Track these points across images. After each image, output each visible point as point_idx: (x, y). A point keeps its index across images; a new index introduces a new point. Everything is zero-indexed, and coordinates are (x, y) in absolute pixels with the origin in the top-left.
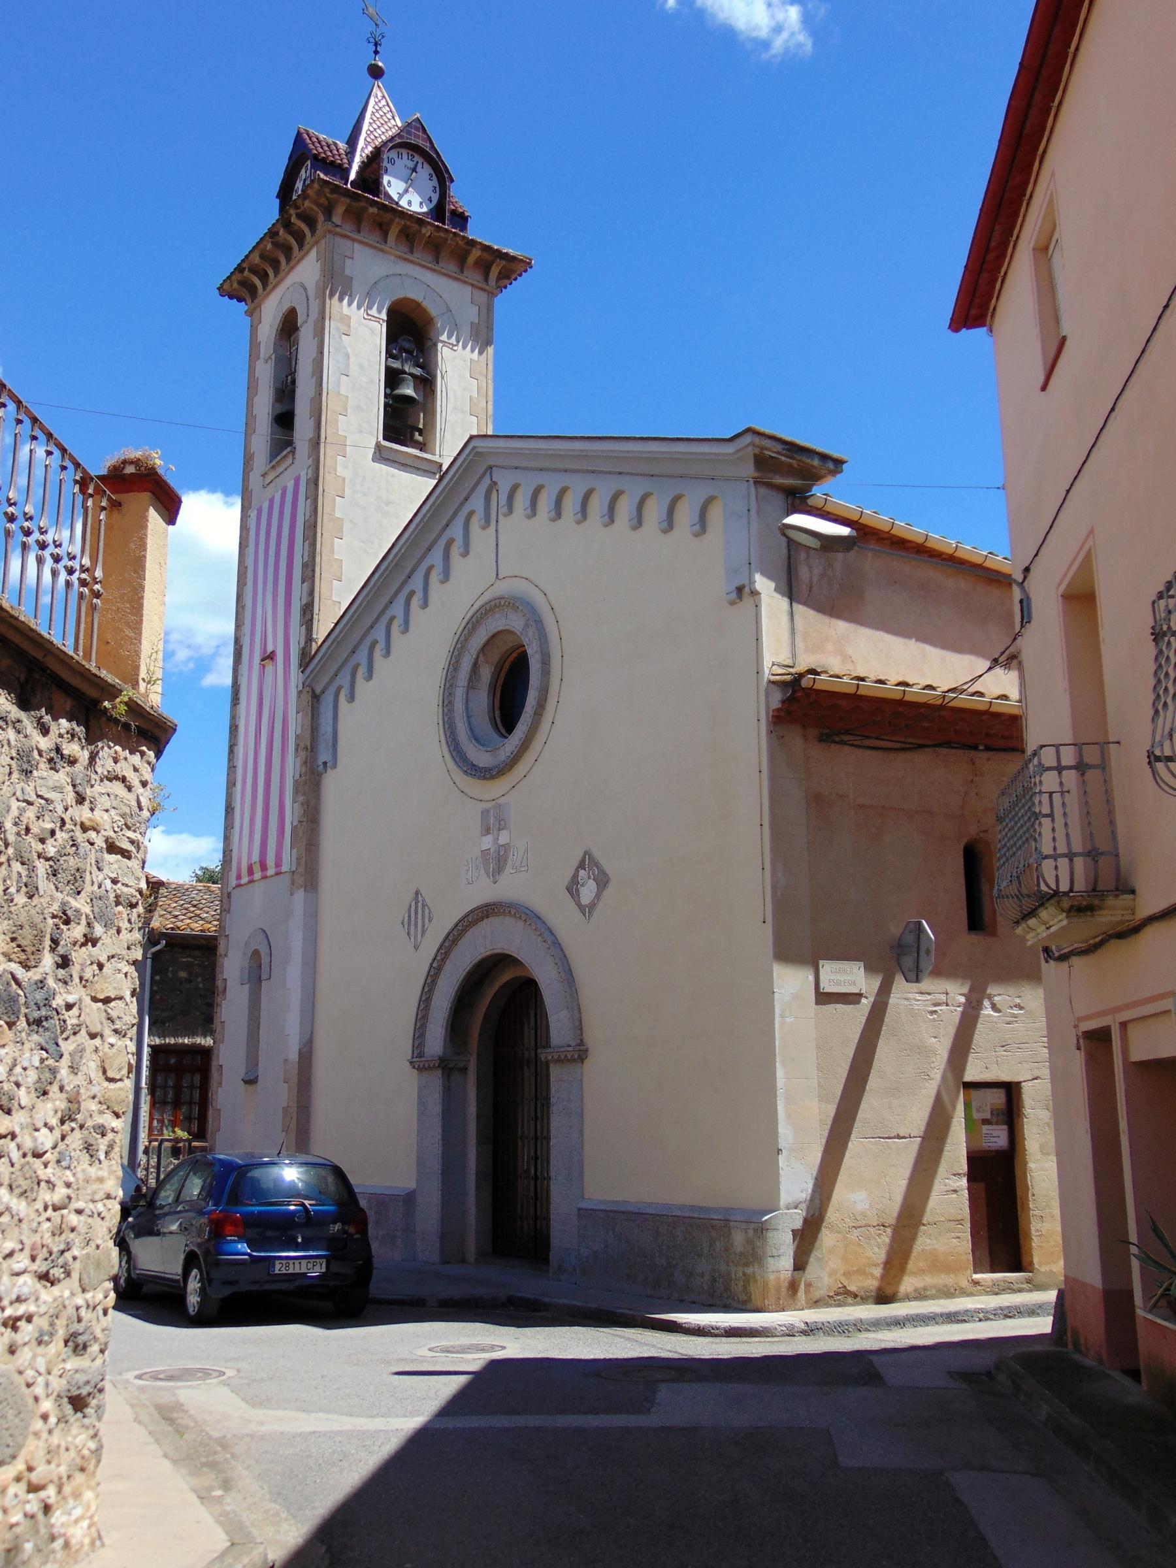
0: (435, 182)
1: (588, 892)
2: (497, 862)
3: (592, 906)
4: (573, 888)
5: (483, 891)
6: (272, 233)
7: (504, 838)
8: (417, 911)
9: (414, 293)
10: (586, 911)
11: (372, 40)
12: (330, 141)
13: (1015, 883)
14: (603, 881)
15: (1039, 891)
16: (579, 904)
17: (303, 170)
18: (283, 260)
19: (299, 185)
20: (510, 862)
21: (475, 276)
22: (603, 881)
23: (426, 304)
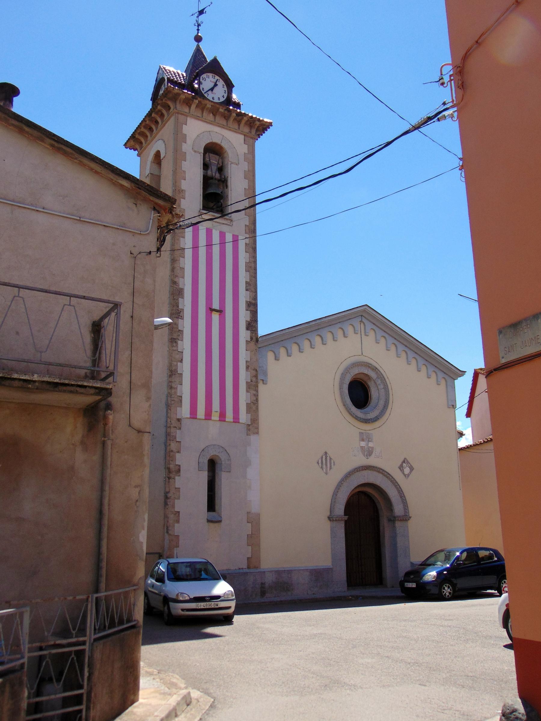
0: (226, 89)
1: (407, 470)
2: (369, 452)
3: (408, 475)
4: (401, 468)
5: (362, 460)
6: (149, 114)
7: (371, 444)
8: (325, 461)
9: (216, 140)
10: (407, 476)
11: (197, 24)
12: (175, 71)
13: (446, 711)
14: (412, 469)
15: (438, 561)
16: (404, 473)
17: (163, 86)
18: (154, 127)
19: (161, 92)
20: (374, 453)
21: (247, 130)
22: (412, 469)
23: (223, 145)
